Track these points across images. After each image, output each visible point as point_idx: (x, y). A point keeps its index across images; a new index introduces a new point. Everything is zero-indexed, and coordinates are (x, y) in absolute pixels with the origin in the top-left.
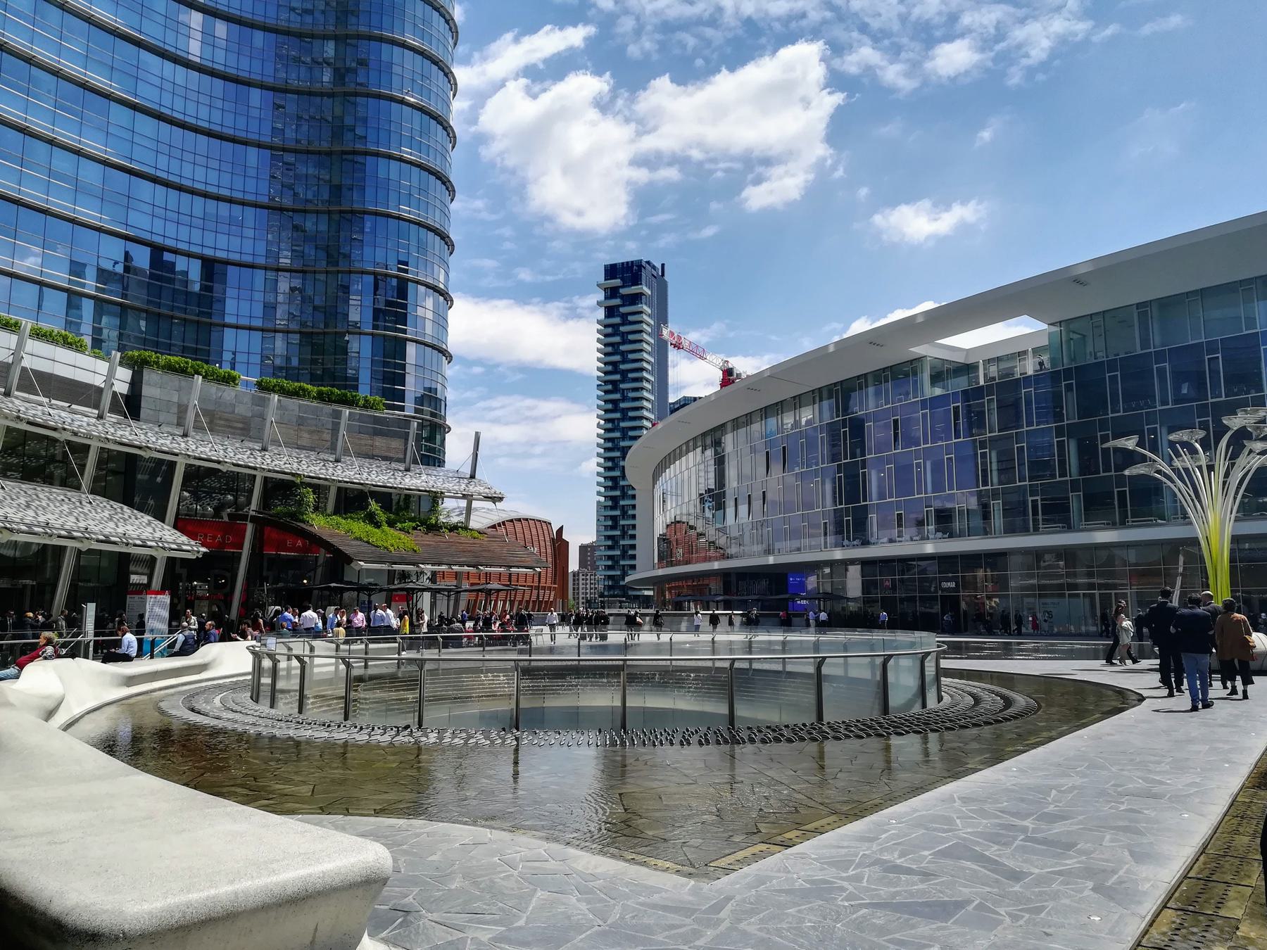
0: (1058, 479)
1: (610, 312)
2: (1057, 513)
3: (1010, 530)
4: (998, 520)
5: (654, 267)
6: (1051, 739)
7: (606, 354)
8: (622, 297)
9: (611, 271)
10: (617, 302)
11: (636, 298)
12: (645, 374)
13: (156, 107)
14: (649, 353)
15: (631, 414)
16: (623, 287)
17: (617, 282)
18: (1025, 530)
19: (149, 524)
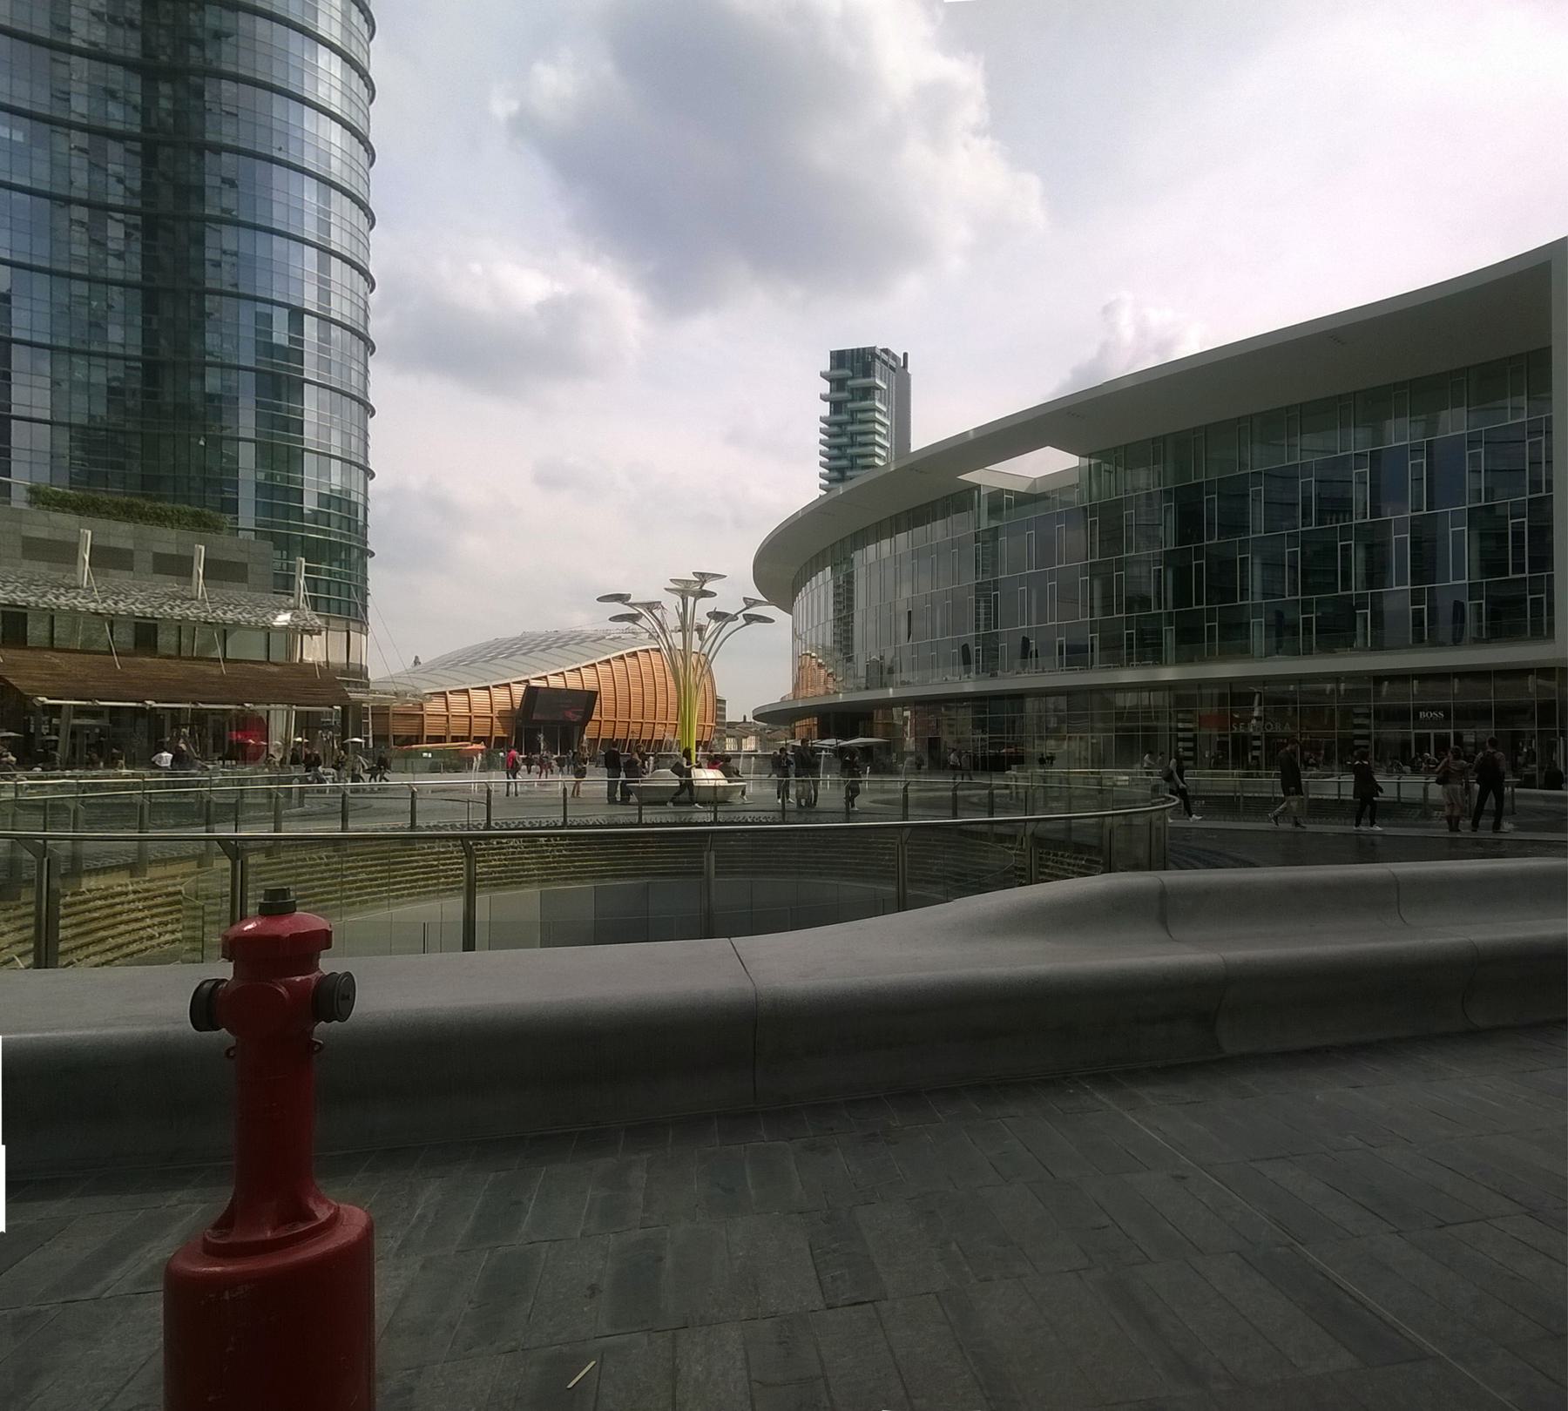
1: (836, 406)
5: (895, 357)
6: (1526, 856)
7: (830, 481)
8: (852, 390)
9: (839, 358)
10: (845, 395)
12: (877, 438)
13: (28, 30)
14: (885, 437)
15: (860, 439)
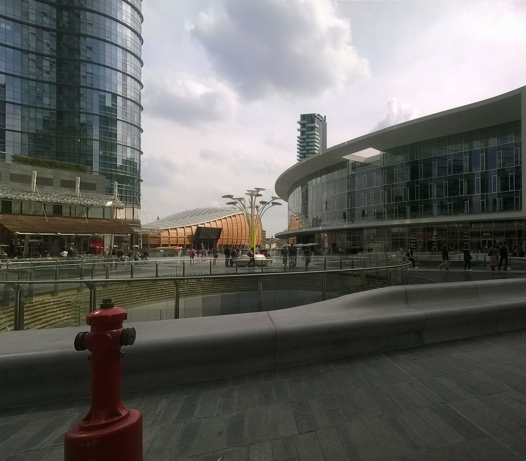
0: (510, 191)
1: (303, 133)
2: (402, 214)
3: (441, 214)
4: (435, 210)
5: (322, 117)
8: (308, 128)
9: (303, 117)
10: (305, 129)
11: (313, 128)
14: (318, 143)
15: (310, 144)
16: (308, 131)
17: (306, 122)
18: (488, 212)
19: (317, 222)
